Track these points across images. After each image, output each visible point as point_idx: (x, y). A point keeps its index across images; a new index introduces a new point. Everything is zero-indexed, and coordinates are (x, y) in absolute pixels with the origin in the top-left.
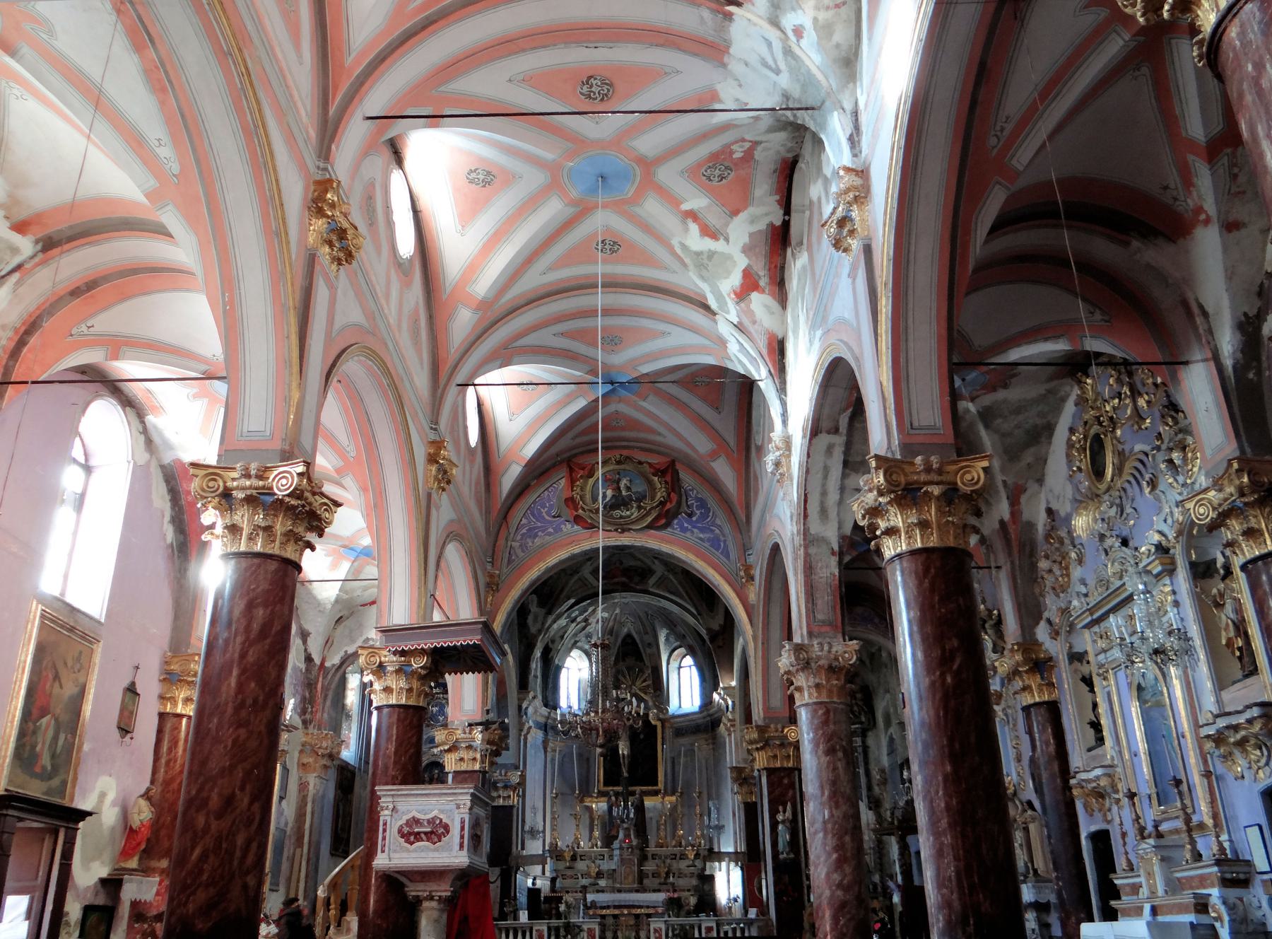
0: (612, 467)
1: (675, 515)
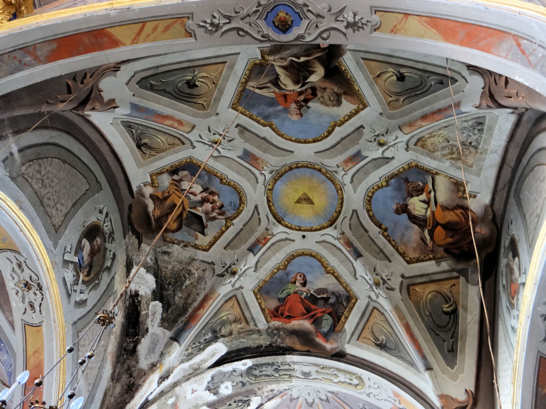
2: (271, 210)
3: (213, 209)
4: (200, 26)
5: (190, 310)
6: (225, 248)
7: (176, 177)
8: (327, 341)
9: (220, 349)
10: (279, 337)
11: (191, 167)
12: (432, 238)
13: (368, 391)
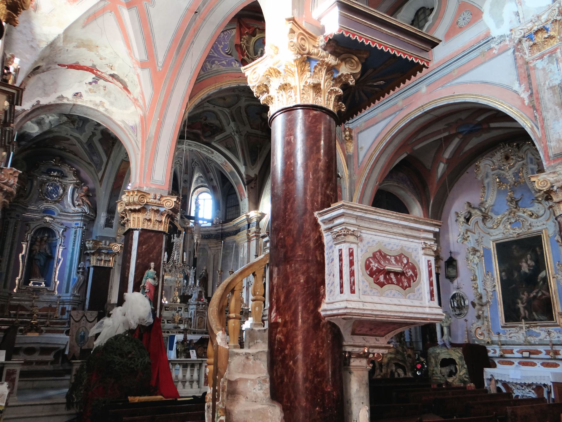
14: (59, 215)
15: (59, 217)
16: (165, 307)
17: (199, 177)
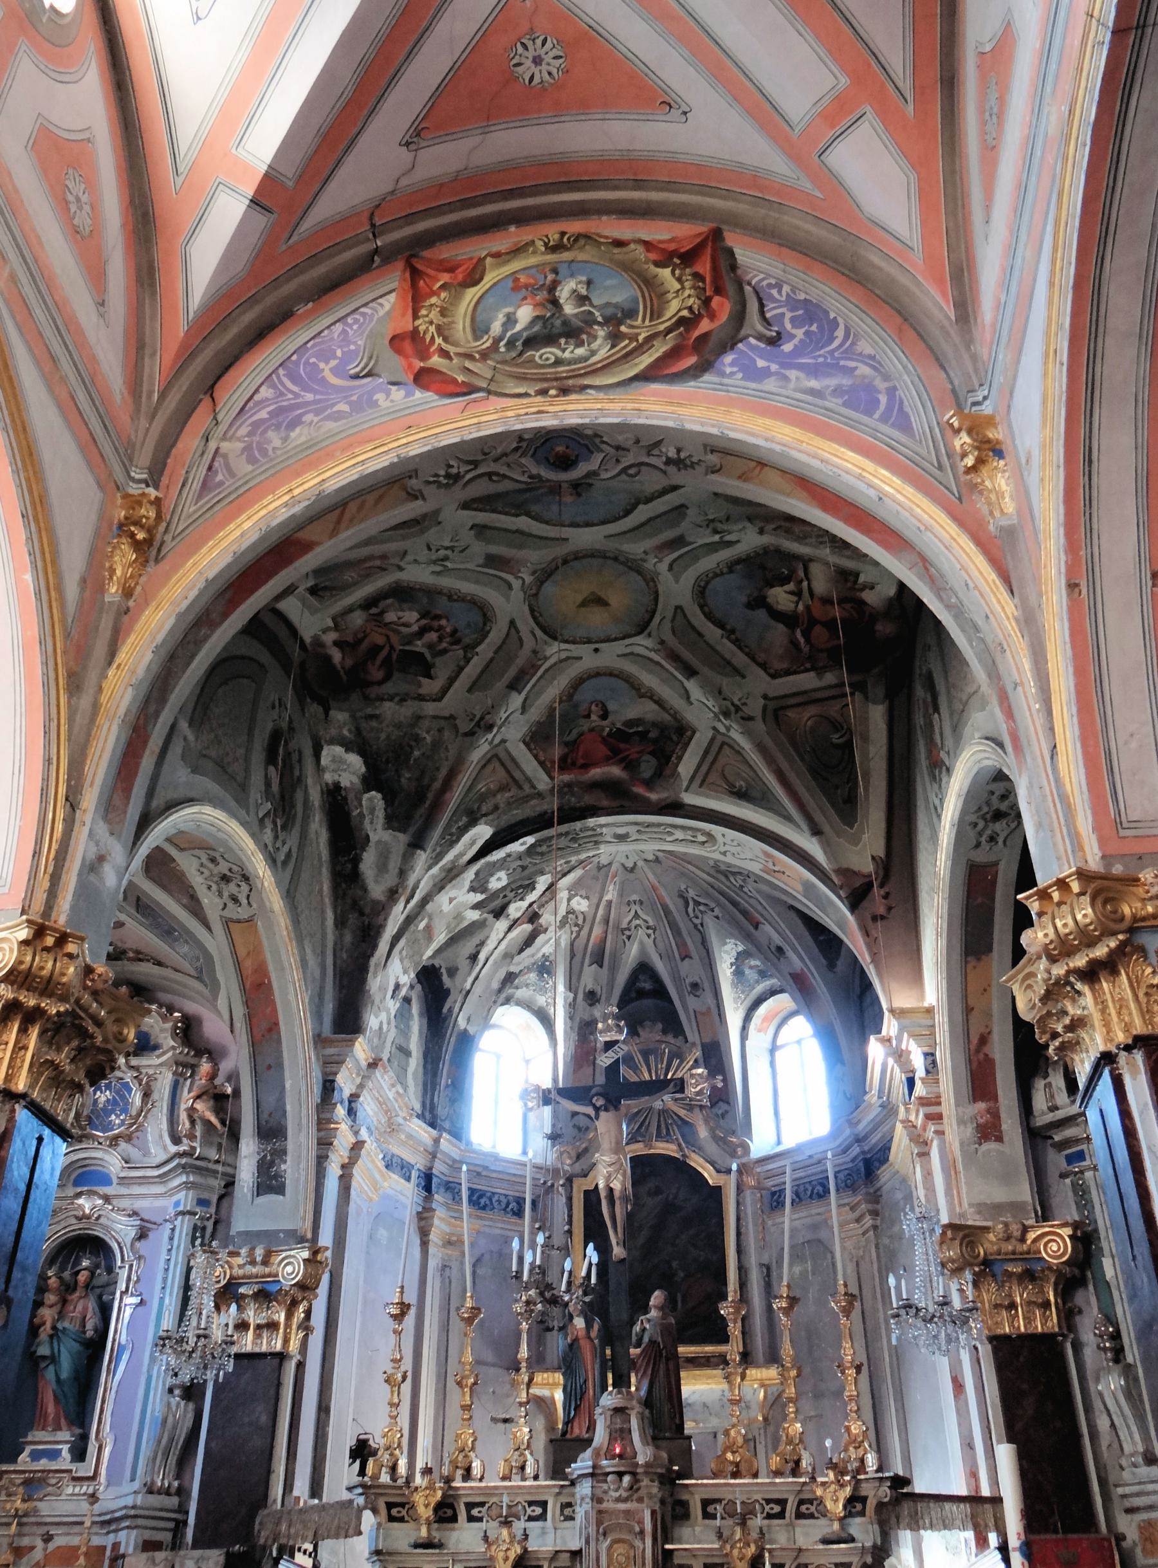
0: (533, 260)
1: (730, 342)
2: (538, 623)
3: (440, 639)
4: (429, 483)
5: (430, 796)
6: (469, 691)
7: (374, 610)
8: (651, 790)
9: (483, 832)
10: (573, 795)
11: (402, 593)
12: (808, 640)
13: (723, 849)
14: (123, 1181)
15: (124, 1191)
16: (470, 1506)
17: (741, 957)
